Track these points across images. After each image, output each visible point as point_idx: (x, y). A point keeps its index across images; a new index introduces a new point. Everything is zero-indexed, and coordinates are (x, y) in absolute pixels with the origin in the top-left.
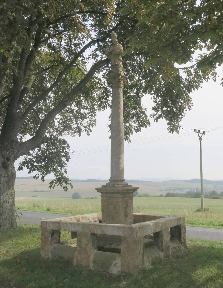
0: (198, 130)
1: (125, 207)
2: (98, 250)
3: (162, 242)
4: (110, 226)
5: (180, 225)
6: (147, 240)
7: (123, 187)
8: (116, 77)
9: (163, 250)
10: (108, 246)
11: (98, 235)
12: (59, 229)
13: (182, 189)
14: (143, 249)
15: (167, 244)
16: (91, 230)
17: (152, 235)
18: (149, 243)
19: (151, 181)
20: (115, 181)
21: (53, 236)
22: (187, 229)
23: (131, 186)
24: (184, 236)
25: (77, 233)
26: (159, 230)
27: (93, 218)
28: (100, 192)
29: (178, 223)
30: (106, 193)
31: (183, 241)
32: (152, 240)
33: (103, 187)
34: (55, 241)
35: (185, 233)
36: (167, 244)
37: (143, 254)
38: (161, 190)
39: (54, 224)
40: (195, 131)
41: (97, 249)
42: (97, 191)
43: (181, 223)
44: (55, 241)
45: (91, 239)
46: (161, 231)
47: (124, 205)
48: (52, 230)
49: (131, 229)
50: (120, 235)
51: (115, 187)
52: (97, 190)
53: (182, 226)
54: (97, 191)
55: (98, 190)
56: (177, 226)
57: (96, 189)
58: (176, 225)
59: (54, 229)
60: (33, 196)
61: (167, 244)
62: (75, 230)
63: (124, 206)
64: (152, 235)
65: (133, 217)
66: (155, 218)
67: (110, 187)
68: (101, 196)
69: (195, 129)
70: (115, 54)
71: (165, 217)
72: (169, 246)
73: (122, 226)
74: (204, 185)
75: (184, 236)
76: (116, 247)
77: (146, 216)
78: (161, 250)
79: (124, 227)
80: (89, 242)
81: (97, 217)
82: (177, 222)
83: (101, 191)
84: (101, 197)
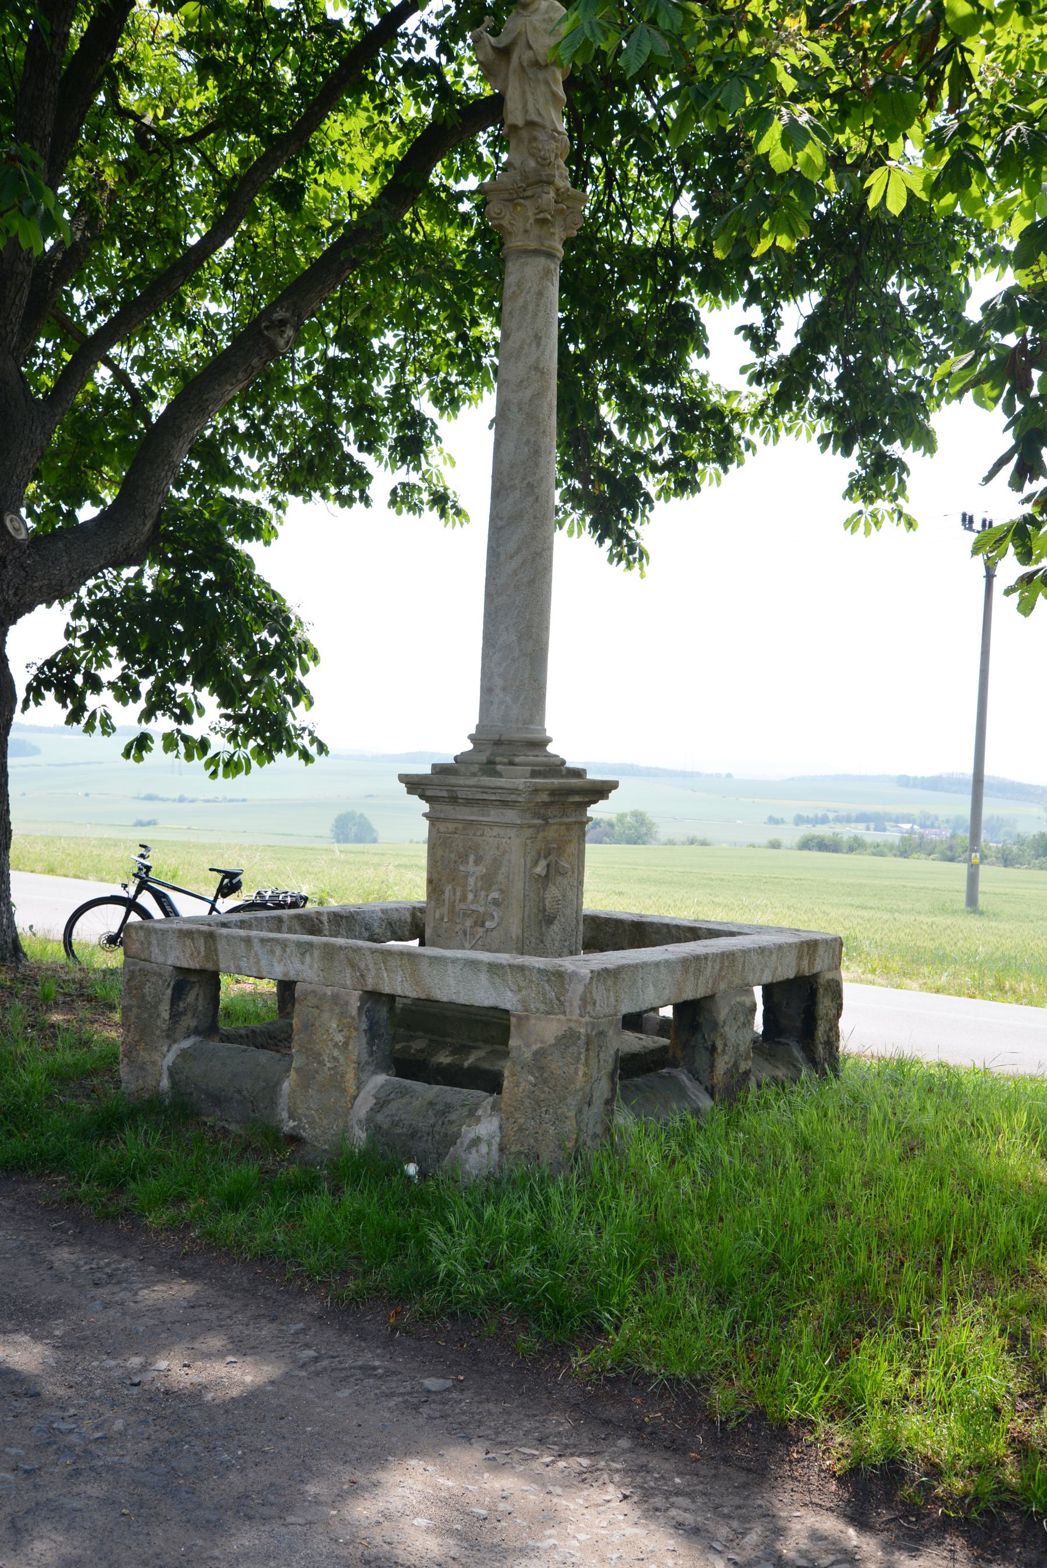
0: (984, 521)
1: (543, 874)
2: (400, 1074)
3: (713, 1049)
4: (455, 961)
5: (815, 976)
6: (634, 1042)
7: (534, 774)
8: (529, 193)
9: (713, 1087)
10: (444, 1059)
11: (399, 1004)
12: (210, 966)
13: (878, 821)
14: (612, 1076)
15: (736, 1065)
16: (362, 976)
17: (667, 1012)
18: (652, 1052)
19: (729, 776)
20: (498, 743)
21: (180, 999)
22: (850, 992)
23: (579, 773)
24: (831, 1029)
25: (299, 987)
26: (700, 993)
27: (390, 924)
28: (422, 797)
29: (805, 963)
30: (453, 800)
31: (821, 1051)
32: (665, 1041)
33: (440, 770)
34: (189, 1021)
35: (839, 1015)
36: (736, 1065)
37: (608, 1102)
38: (773, 821)
39: (188, 942)
40: (964, 524)
41: (393, 1071)
42: (409, 793)
43: (817, 968)
44: (189, 1021)
45: (364, 1018)
46: (710, 998)
47: (536, 863)
48: (179, 969)
49: (559, 976)
50: (502, 1006)
51: (499, 775)
52: (407, 784)
53: (822, 981)
54: (409, 793)
55: (414, 785)
56: (796, 978)
57: (404, 779)
58: (792, 977)
59: (185, 965)
60: (140, 824)
61: (736, 1062)
62: (286, 974)
63: (540, 869)
64: (667, 1012)
65: (581, 928)
66: (693, 933)
67: (474, 775)
68: (425, 815)
69: (964, 515)
70: (525, 64)
71: (740, 934)
72: (747, 1073)
73: (512, 961)
74: (989, 809)
75: (831, 1029)
76: (487, 1066)
77: (651, 924)
78: (706, 1089)
79: (521, 968)
80: (355, 1034)
81: (409, 920)
82: (800, 958)
83: (428, 793)
84: (426, 823)
